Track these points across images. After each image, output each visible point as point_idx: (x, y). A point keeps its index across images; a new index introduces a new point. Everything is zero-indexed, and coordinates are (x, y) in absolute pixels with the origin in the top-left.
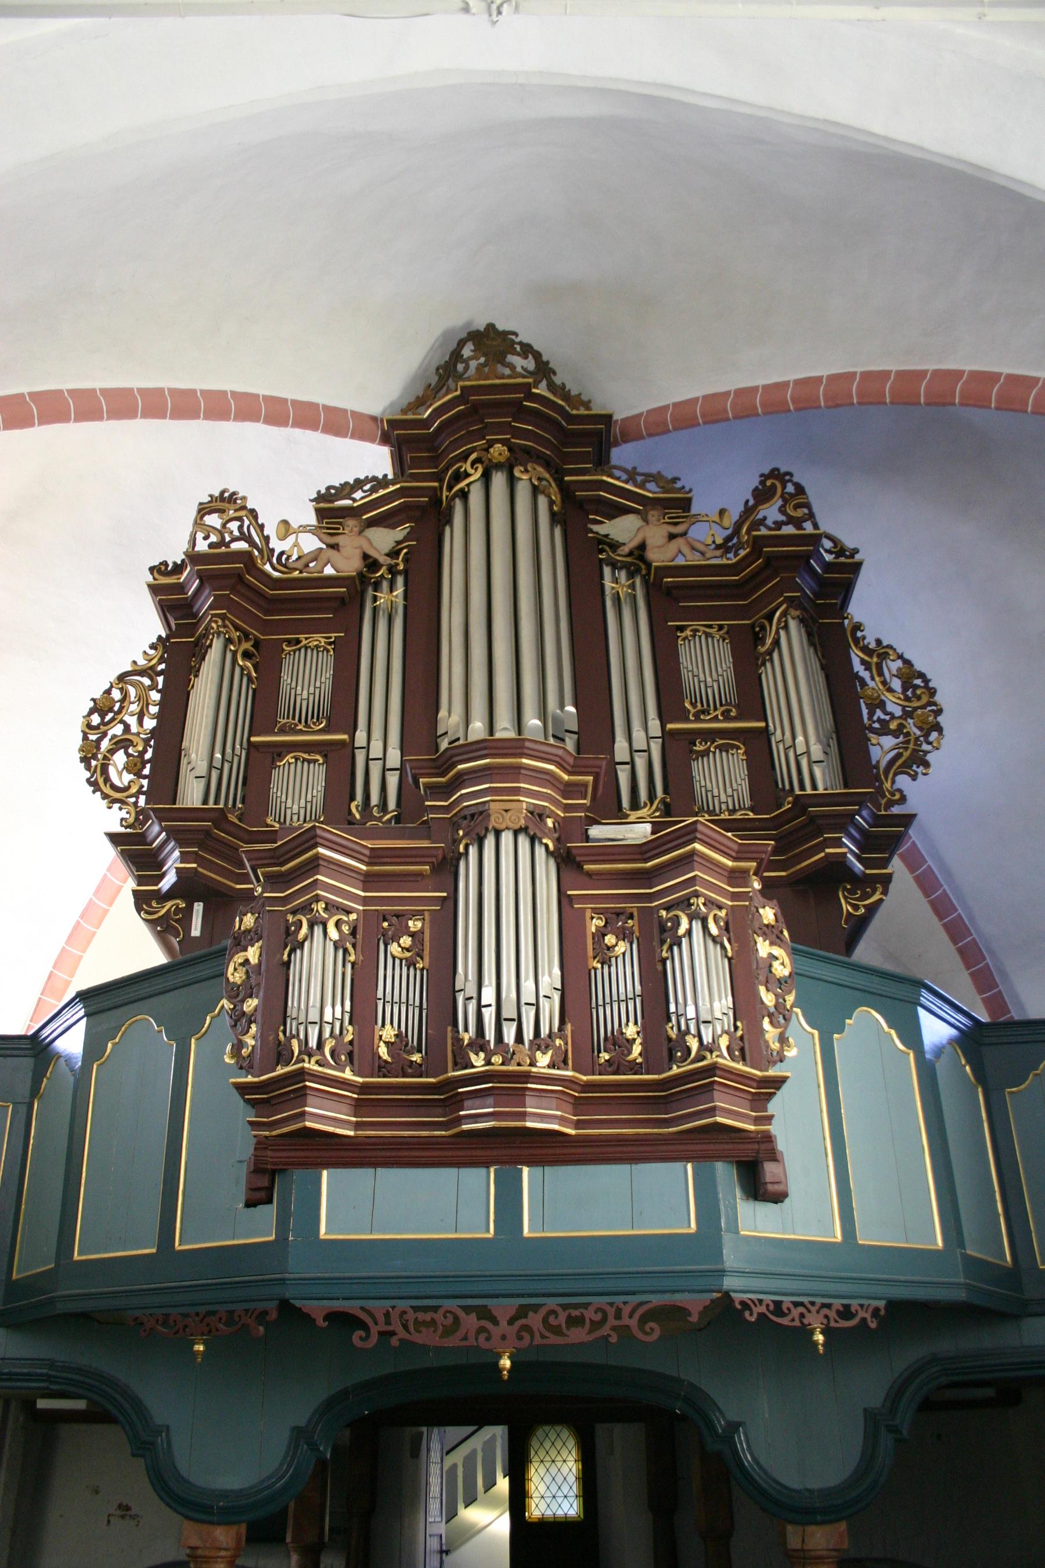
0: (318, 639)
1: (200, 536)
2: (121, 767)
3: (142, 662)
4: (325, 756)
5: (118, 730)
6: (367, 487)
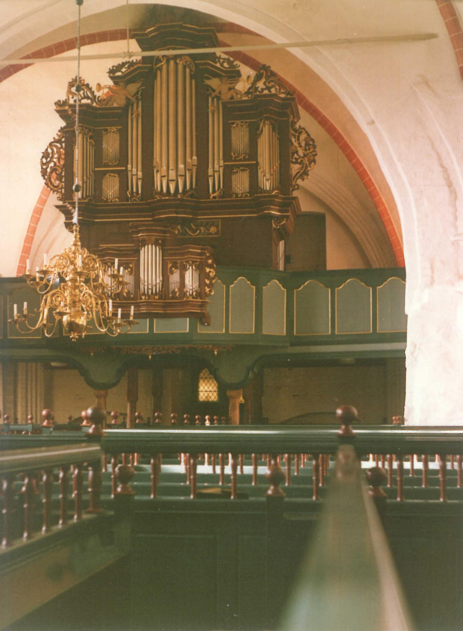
0: (114, 129)
1: (71, 96)
2: (55, 178)
3: (57, 138)
4: (118, 175)
5: (52, 164)
6: (126, 66)
